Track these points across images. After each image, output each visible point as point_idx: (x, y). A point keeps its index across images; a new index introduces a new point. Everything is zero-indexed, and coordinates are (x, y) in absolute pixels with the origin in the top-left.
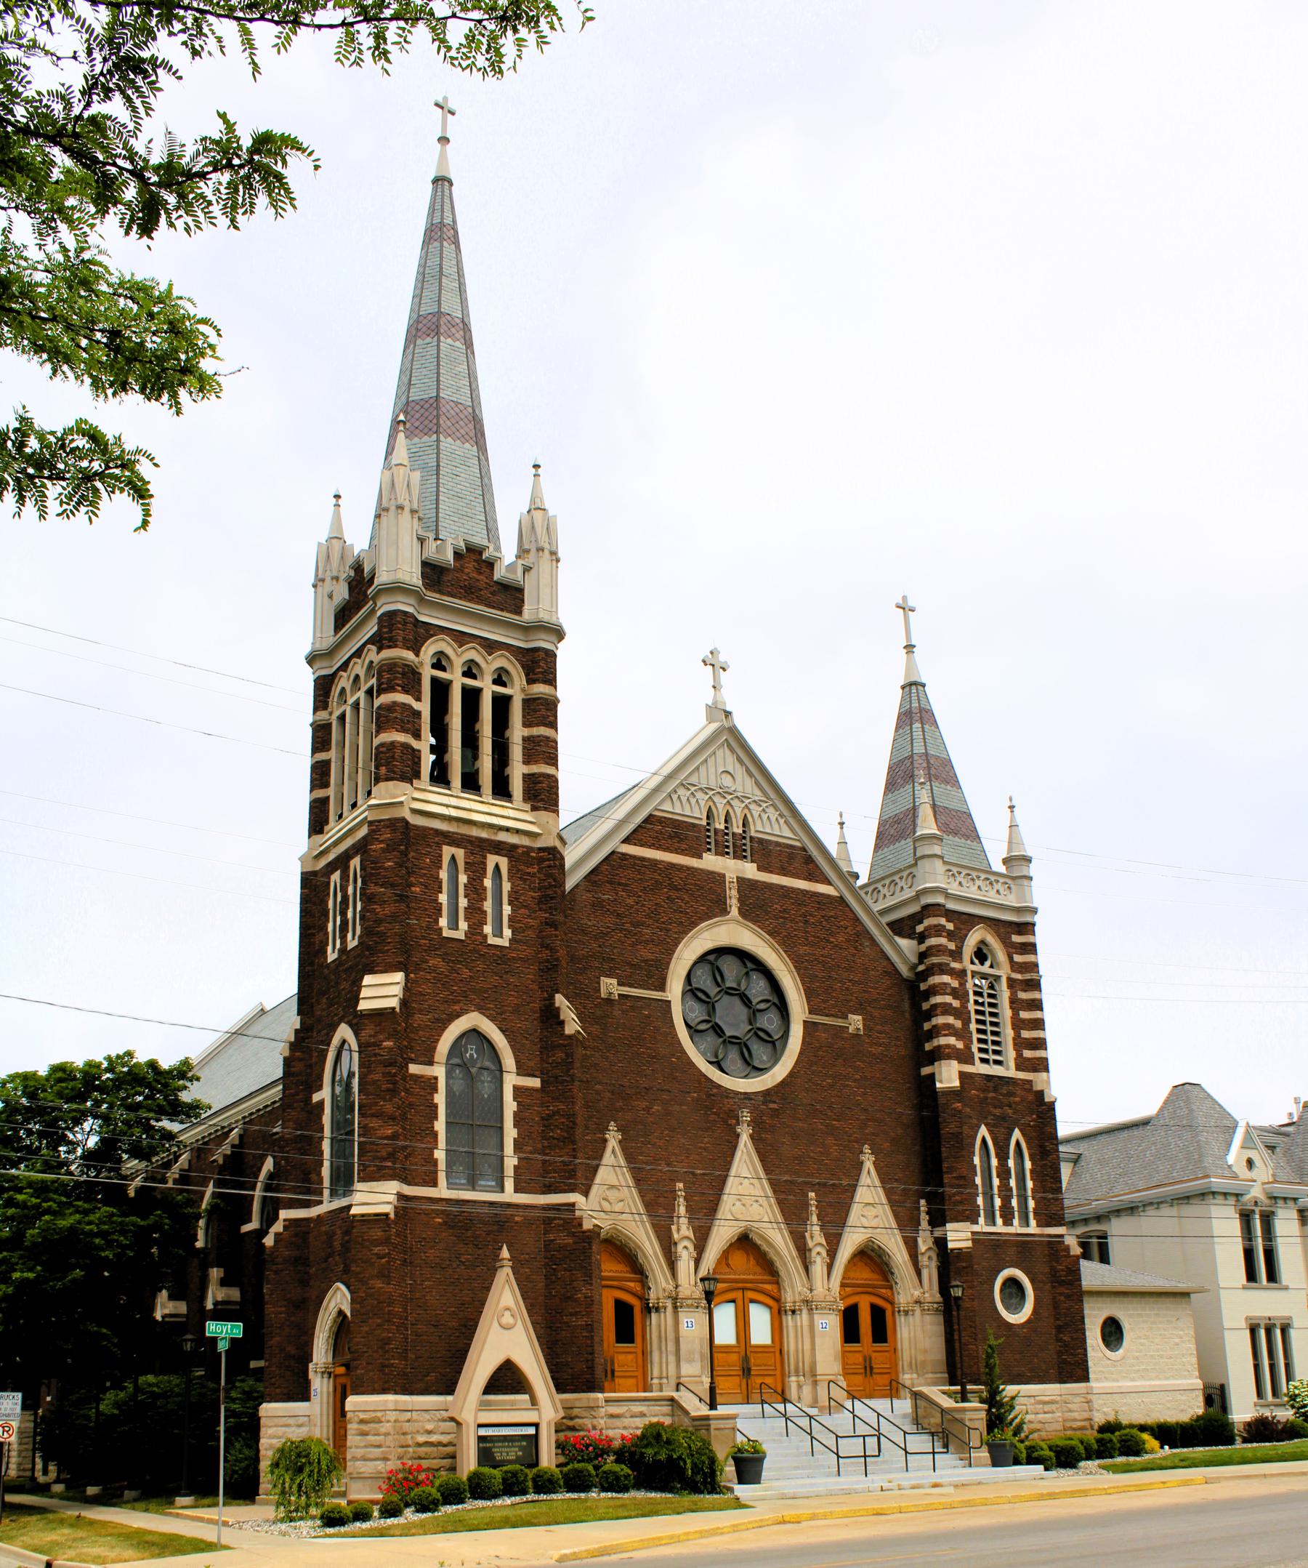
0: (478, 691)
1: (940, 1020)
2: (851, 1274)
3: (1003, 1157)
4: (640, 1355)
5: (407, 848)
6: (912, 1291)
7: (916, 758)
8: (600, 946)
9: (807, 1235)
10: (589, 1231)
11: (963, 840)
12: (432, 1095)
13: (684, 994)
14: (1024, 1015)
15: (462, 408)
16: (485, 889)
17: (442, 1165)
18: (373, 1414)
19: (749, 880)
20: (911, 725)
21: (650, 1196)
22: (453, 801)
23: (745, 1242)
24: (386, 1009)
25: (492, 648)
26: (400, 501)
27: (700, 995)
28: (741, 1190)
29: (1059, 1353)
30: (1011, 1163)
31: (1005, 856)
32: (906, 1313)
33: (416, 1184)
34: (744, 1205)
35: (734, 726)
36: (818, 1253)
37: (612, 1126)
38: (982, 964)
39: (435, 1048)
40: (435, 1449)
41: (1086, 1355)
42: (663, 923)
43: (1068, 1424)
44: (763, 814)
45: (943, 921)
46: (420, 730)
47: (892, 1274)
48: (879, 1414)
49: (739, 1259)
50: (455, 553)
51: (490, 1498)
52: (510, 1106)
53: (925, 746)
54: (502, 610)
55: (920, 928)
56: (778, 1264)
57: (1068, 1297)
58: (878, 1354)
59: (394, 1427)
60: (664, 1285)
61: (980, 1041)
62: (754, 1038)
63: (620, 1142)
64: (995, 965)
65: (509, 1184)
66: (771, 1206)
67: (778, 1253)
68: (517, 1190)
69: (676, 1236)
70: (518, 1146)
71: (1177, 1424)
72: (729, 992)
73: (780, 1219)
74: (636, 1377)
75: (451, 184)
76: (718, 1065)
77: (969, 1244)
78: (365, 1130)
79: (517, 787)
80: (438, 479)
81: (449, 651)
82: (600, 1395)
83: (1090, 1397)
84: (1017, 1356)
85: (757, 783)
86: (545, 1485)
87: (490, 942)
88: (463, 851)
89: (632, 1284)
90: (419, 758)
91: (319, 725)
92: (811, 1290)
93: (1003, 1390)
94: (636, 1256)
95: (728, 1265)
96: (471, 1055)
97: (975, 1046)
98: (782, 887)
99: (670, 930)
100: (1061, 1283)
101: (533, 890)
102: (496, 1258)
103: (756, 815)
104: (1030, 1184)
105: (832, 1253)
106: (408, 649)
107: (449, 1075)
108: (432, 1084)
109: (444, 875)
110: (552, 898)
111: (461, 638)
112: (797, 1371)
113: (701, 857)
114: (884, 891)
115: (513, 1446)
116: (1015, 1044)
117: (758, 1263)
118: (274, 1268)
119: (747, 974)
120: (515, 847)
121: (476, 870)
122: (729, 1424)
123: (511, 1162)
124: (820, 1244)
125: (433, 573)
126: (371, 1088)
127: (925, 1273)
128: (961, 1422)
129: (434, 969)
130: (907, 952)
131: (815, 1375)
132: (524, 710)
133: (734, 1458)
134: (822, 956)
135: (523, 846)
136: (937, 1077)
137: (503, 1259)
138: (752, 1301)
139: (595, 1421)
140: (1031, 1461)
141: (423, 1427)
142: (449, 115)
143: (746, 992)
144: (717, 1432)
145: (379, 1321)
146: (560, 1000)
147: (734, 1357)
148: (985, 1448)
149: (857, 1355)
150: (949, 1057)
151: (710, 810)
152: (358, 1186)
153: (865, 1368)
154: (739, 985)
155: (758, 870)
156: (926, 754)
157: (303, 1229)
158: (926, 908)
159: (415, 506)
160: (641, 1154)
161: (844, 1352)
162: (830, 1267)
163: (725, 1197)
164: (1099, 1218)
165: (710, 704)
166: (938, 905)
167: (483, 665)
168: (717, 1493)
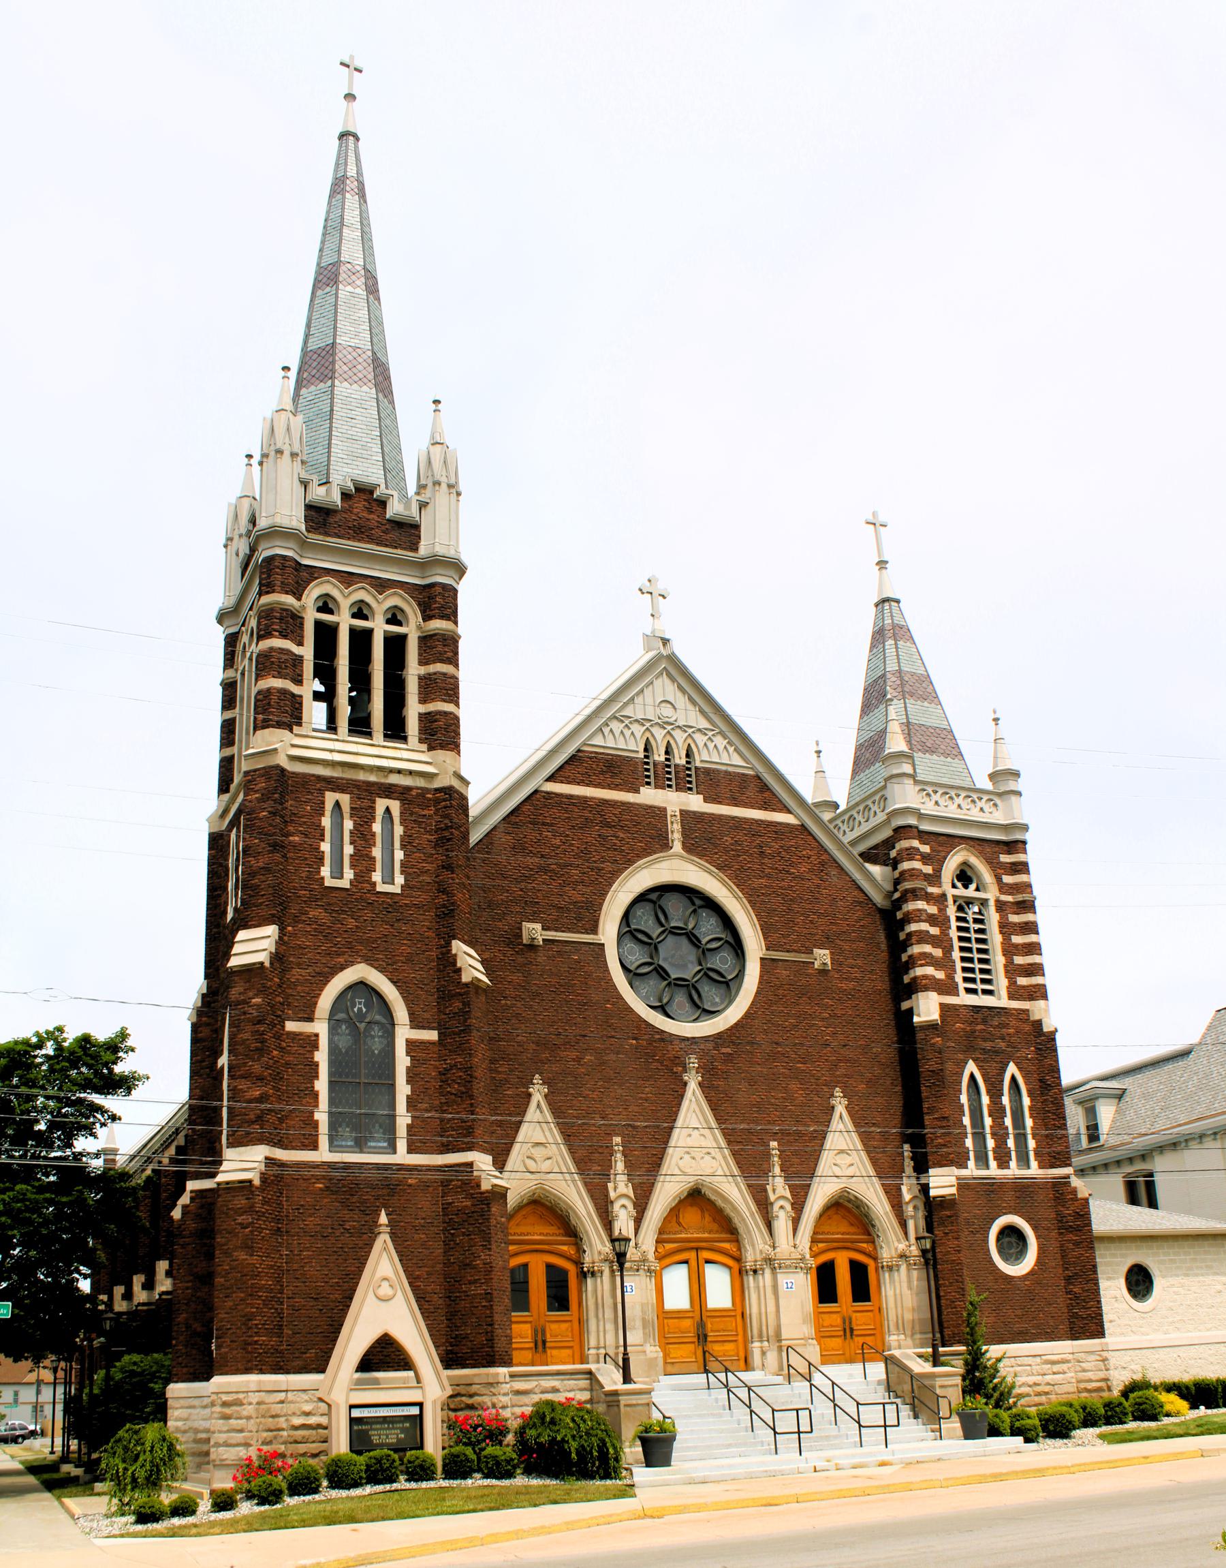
0: (369, 633)
1: (916, 949)
2: (826, 1228)
3: (995, 1094)
4: (576, 1324)
5: (282, 797)
6: (896, 1244)
7: (888, 675)
8: (521, 890)
9: (769, 1188)
10: (487, 1191)
11: (942, 758)
12: (312, 1052)
13: (620, 937)
14: (1017, 939)
15: (360, 351)
16: (374, 835)
17: (324, 1128)
18: (235, 1396)
19: (694, 813)
20: (884, 643)
21: (581, 1153)
22: (406, 755)
23: (696, 1197)
24: (254, 964)
25: (385, 587)
26: (279, 445)
27: (640, 936)
28: (690, 1142)
29: (1070, 1307)
30: (1005, 1100)
31: (991, 771)
32: (890, 1268)
33: (293, 1148)
34: (694, 1158)
35: (673, 653)
36: (782, 1207)
37: (537, 1079)
38: (966, 887)
39: (316, 1003)
40: (314, 1432)
41: (1100, 1308)
42: (595, 862)
43: (1082, 1385)
44: (709, 743)
45: (915, 843)
46: (301, 675)
47: (873, 1226)
48: (833, 1383)
49: (691, 1216)
50: (342, 494)
51: (348, 1487)
52: (402, 1061)
53: (899, 662)
54: (396, 548)
55: (893, 854)
56: (736, 1221)
57: (1077, 1244)
58: (861, 1315)
59: (257, 1410)
60: (600, 1247)
61: (964, 969)
62: (705, 979)
63: (546, 1096)
64: (981, 887)
65: (402, 1145)
66: (724, 1157)
67: (735, 1209)
68: (411, 1150)
69: (612, 1195)
70: (411, 1103)
71: (1218, 1380)
72: (674, 932)
73: (736, 1171)
74: (571, 1347)
75: (357, 139)
76: (663, 1009)
77: (953, 1190)
78: (235, 1094)
79: (413, 726)
80: (331, 423)
81: (335, 593)
82: (503, 1371)
83: (1105, 1354)
84: (1019, 1312)
85: (702, 712)
86: (421, 1472)
87: (379, 889)
88: (348, 796)
89: (565, 1248)
90: (301, 704)
91: (226, 684)
92: (774, 1247)
93: (987, 1351)
94: (568, 1217)
95: (679, 1224)
96: (360, 1009)
97: (959, 976)
98: (733, 818)
99: (603, 869)
100: (1070, 1229)
101: (429, 832)
102: (375, 1223)
103: (701, 745)
104: (1029, 1123)
105: (798, 1206)
106: (287, 593)
107: (333, 1031)
108: (311, 1042)
109: (326, 822)
110: (449, 840)
111: (348, 579)
112: (760, 1336)
113: (637, 791)
114: (859, 818)
115: (393, 1428)
116: (1007, 972)
117: (714, 1220)
118: (181, 1241)
119: (694, 911)
120: (408, 789)
121: (364, 816)
122: (643, 1399)
123: (403, 1120)
124: (783, 1197)
125: (318, 516)
126: (240, 1048)
127: (911, 1224)
128: (931, 1389)
129: (315, 921)
130: (879, 878)
131: (780, 1341)
132: (420, 647)
133: (641, 1438)
134: (781, 888)
135: (418, 788)
136: (915, 1011)
137: (381, 1225)
138: (708, 1262)
139: (495, 1399)
140: (1015, 1432)
141: (300, 1409)
142: (356, 73)
143: (695, 932)
144: (628, 1409)
145: (242, 1295)
146: (458, 947)
147: (687, 1323)
148: (955, 1418)
149: (834, 1316)
150: (926, 989)
151: (668, 745)
152: (228, 1153)
153: (845, 1330)
154: (686, 924)
155: (705, 801)
156: (900, 671)
157: (209, 1200)
158: (897, 830)
159: (296, 449)
160: (571, 1107)
161: (818, 1314)
162: (796, 1222)
163: (670, 1151)
164: (1144, 1156)
165: (649, 634)
166: (910, 826)
167: (374, 604)
168: (611, 1479)
